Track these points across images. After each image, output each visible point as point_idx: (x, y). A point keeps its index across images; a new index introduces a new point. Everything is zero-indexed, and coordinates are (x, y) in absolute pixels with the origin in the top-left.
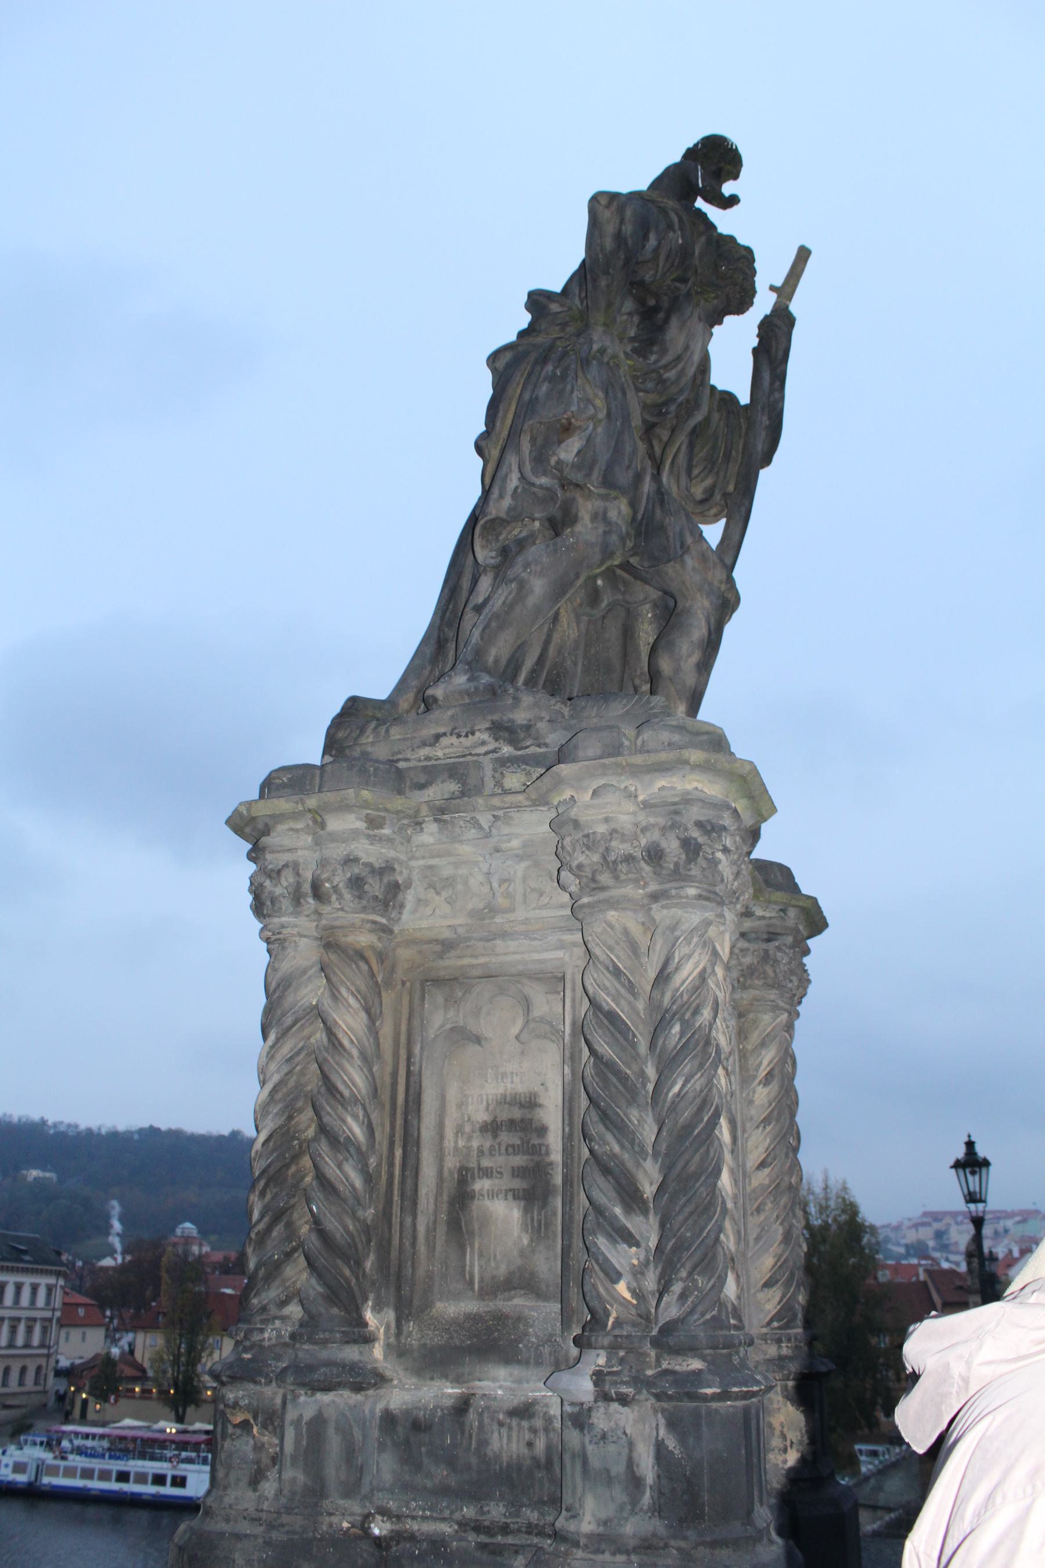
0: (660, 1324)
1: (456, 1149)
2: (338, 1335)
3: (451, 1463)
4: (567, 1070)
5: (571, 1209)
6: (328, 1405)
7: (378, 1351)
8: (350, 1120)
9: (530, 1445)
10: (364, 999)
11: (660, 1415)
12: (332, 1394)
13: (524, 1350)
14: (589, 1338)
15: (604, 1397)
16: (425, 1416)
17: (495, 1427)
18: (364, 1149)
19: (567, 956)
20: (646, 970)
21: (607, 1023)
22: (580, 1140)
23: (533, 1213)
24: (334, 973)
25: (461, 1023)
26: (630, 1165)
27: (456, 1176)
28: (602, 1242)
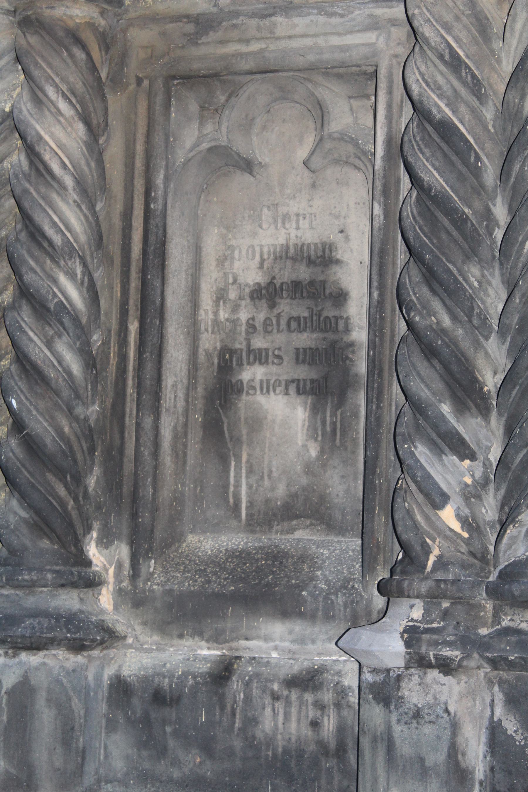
1: (216, 322)
2: (49, 576)
3: (207, 747)
4: (378, 210)
5: (378, 407)
6: (37, 669)
7: (106, 599)
8: (63, 279)
9: (315, 724)
10: (81, 102)
11: (496, 688)
12: (42, 653)
13: (309, 599)
14: (399, 583)
15: (419, 662)
16: (171, 686)
17: (268, 700)
18: (84, 320)
19: (381, 40)
20: (499, 61)
21: (438, 140)
22: (393, 311)
24: (36, 64)
25: (224, 142)
26: (466, 345)
27: (216, 361)
28: (422, 452)
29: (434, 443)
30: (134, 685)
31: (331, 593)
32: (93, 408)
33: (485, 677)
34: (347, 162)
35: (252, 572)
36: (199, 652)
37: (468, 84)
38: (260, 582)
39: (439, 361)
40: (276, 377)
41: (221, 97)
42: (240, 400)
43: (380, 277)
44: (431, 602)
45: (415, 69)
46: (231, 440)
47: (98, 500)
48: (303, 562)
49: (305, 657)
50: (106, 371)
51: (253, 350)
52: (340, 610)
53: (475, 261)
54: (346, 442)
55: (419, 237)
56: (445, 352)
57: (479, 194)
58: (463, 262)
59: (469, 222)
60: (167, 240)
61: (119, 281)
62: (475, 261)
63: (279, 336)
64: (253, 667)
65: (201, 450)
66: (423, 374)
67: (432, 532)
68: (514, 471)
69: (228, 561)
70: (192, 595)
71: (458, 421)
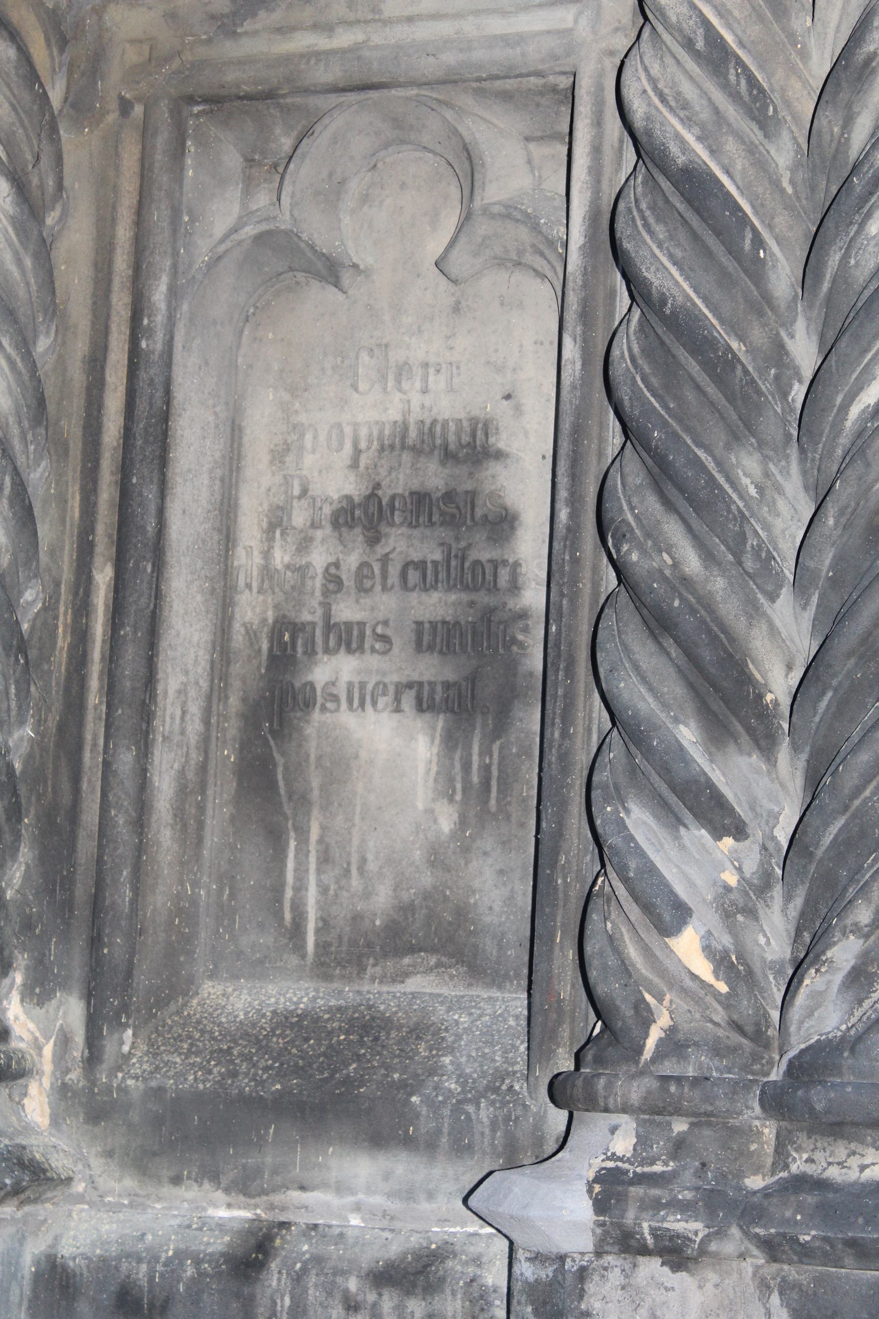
0: (791, 1054)
1: (267, 571)
5: (564, 734)
7: (36, 1104)
11: (775, 1299)
13: (424, 1111)
16: (151, 1279)
19: (584, 22)
20: (804, 55)
21: (681, 206)
23: (468, 747)
25: (285, 222)
26: (730, 609)
27: (265, 646)
28: (640, 822)
29: (665, 805)
30: (82, 1275)
31: (466, 1101)
32: (21, 732)
33: (755, 1274)
34: (520, 264)
35: (319, 1056)
36: (211, 1212)
37: (741, 98)
38: (332, 1076)
39: (676, 642)
40: (379, 678)
41: (283, 140)
42: (308, 722)
43: (573, 480)
44: (651, 1122)
45: (640, 70)
46: (290, 798)
47: (28, 911)
48: (419, 1038)
49: (413, 1226)
50: (49, 662)
51: (335, 624)
52: (482, 1134)
53: (752, 445)
54: (509, 803)
55: (641, 397)
56: (688, 622)
57: (761, 314)
58: (728, 447)
59: (739, 367)
60: (173, 411)
61: (77, 487)
62: (752, 445)
63: (385, 598)
64: (311, 1245)
65: (233, 819)
66: (644, 666)
67: (656, 980)
68: (821, 860)
69: (274, 1035)
70: (199, 1099)
71: (711, 761)
